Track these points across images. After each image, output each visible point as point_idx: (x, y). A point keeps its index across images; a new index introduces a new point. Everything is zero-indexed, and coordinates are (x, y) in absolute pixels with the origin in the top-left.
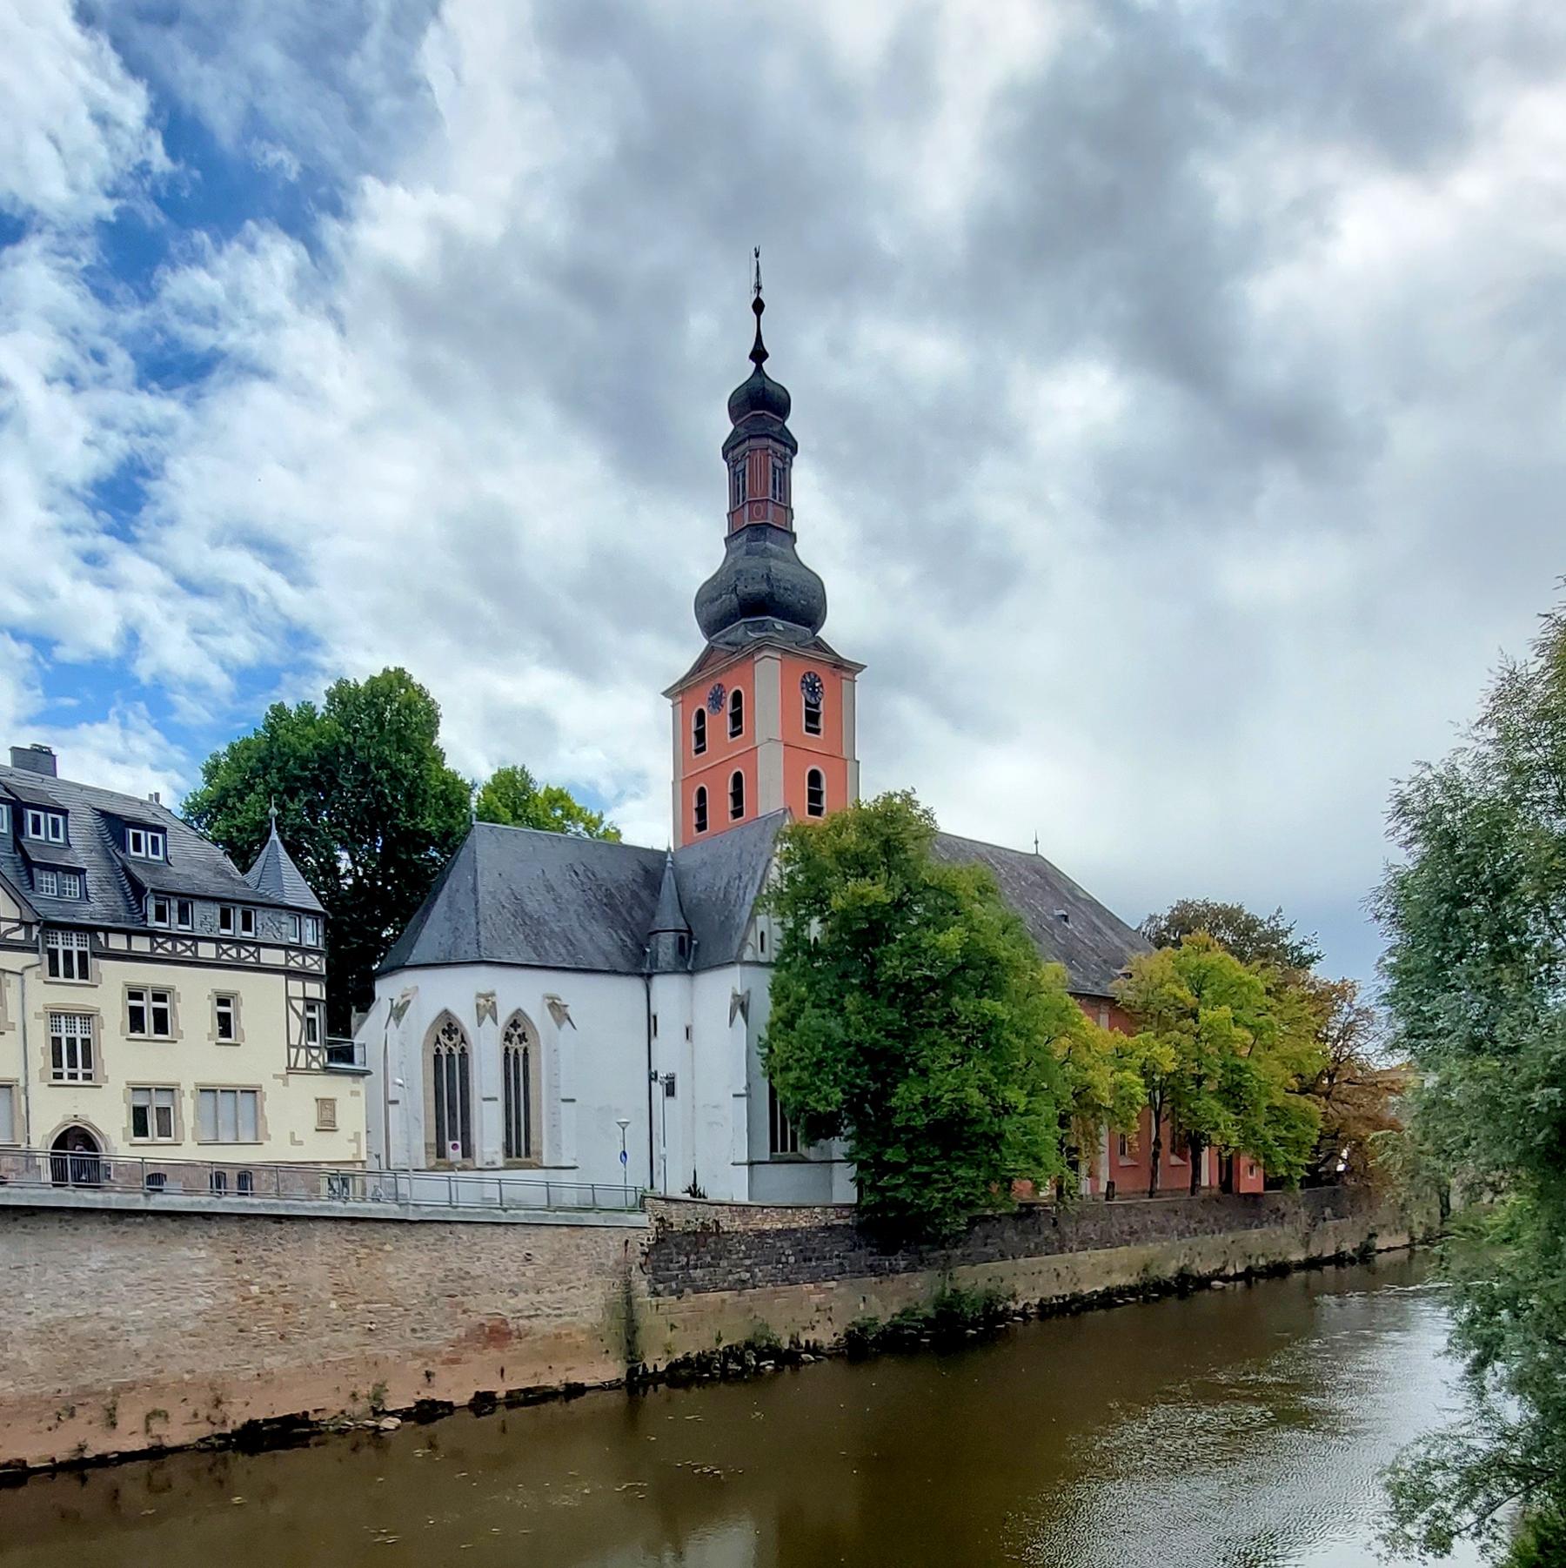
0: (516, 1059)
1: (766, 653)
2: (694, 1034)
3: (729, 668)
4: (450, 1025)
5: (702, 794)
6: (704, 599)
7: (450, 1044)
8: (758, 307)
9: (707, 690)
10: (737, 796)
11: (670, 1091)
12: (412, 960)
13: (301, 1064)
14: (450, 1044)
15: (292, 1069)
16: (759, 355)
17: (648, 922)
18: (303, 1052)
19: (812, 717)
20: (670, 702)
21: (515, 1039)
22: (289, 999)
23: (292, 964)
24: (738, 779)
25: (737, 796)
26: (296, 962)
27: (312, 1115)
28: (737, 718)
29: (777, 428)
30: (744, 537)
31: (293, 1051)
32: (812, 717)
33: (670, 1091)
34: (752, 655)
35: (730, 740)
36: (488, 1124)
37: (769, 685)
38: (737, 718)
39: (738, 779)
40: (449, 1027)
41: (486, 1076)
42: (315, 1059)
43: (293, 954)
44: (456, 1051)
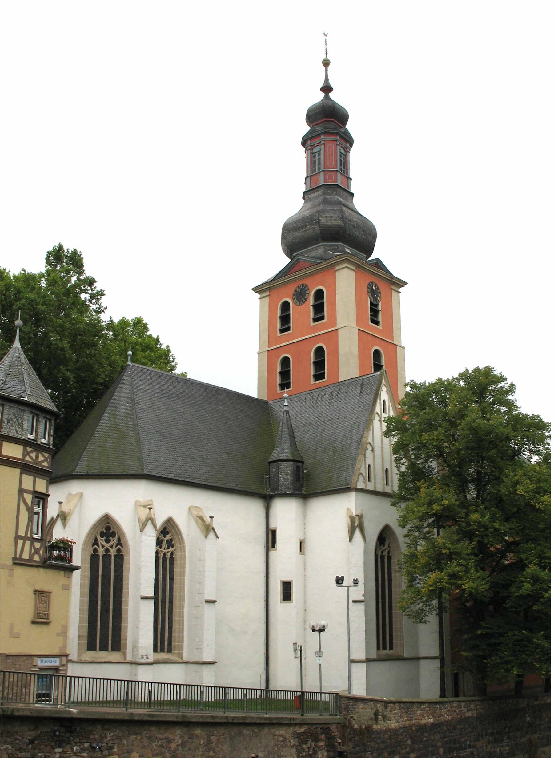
0: (106, 567)
1: (346, 265)
2: (308, 546)
3: (312, 274)
4: (108, 528)
5: (286, 362)
6: (288, 230)
7: (107, 545)
8: (326, 63)
9: (292, 289)
10: (319, 364)
11: (287, 595)
12: (79, 470)
13: (26, 556)
14: (107, 545)
15: (18, 562)
16: (327, 89)
17: (260, 452)
18: (28, 543)
19: (375, 312)
20: (258, 296)
21: (164, 544)
22: (21, 491)
23: (28, 458)
24: (320, 351)
25: (319, 364)
26: (32, 457)
27: (27, 607)
28: (319, 308)
29: (342, 130)
30: (320, 192)
31: (20, 542)
32: (375, 312)
33: (287, 595)
34: (333, 266)
35: (312, 324)
36: (139, 621)
37: (345, 287)
38: (319, 308)
39: (320, 351)
40: (107, 529)
41: (140, 575)
42: (37, 552)
43: (29, 449)
44: (113, 552)
